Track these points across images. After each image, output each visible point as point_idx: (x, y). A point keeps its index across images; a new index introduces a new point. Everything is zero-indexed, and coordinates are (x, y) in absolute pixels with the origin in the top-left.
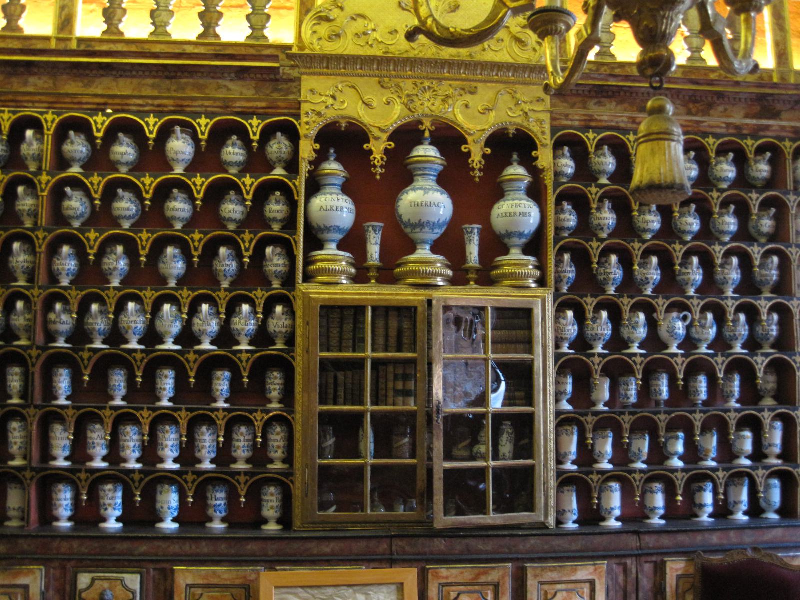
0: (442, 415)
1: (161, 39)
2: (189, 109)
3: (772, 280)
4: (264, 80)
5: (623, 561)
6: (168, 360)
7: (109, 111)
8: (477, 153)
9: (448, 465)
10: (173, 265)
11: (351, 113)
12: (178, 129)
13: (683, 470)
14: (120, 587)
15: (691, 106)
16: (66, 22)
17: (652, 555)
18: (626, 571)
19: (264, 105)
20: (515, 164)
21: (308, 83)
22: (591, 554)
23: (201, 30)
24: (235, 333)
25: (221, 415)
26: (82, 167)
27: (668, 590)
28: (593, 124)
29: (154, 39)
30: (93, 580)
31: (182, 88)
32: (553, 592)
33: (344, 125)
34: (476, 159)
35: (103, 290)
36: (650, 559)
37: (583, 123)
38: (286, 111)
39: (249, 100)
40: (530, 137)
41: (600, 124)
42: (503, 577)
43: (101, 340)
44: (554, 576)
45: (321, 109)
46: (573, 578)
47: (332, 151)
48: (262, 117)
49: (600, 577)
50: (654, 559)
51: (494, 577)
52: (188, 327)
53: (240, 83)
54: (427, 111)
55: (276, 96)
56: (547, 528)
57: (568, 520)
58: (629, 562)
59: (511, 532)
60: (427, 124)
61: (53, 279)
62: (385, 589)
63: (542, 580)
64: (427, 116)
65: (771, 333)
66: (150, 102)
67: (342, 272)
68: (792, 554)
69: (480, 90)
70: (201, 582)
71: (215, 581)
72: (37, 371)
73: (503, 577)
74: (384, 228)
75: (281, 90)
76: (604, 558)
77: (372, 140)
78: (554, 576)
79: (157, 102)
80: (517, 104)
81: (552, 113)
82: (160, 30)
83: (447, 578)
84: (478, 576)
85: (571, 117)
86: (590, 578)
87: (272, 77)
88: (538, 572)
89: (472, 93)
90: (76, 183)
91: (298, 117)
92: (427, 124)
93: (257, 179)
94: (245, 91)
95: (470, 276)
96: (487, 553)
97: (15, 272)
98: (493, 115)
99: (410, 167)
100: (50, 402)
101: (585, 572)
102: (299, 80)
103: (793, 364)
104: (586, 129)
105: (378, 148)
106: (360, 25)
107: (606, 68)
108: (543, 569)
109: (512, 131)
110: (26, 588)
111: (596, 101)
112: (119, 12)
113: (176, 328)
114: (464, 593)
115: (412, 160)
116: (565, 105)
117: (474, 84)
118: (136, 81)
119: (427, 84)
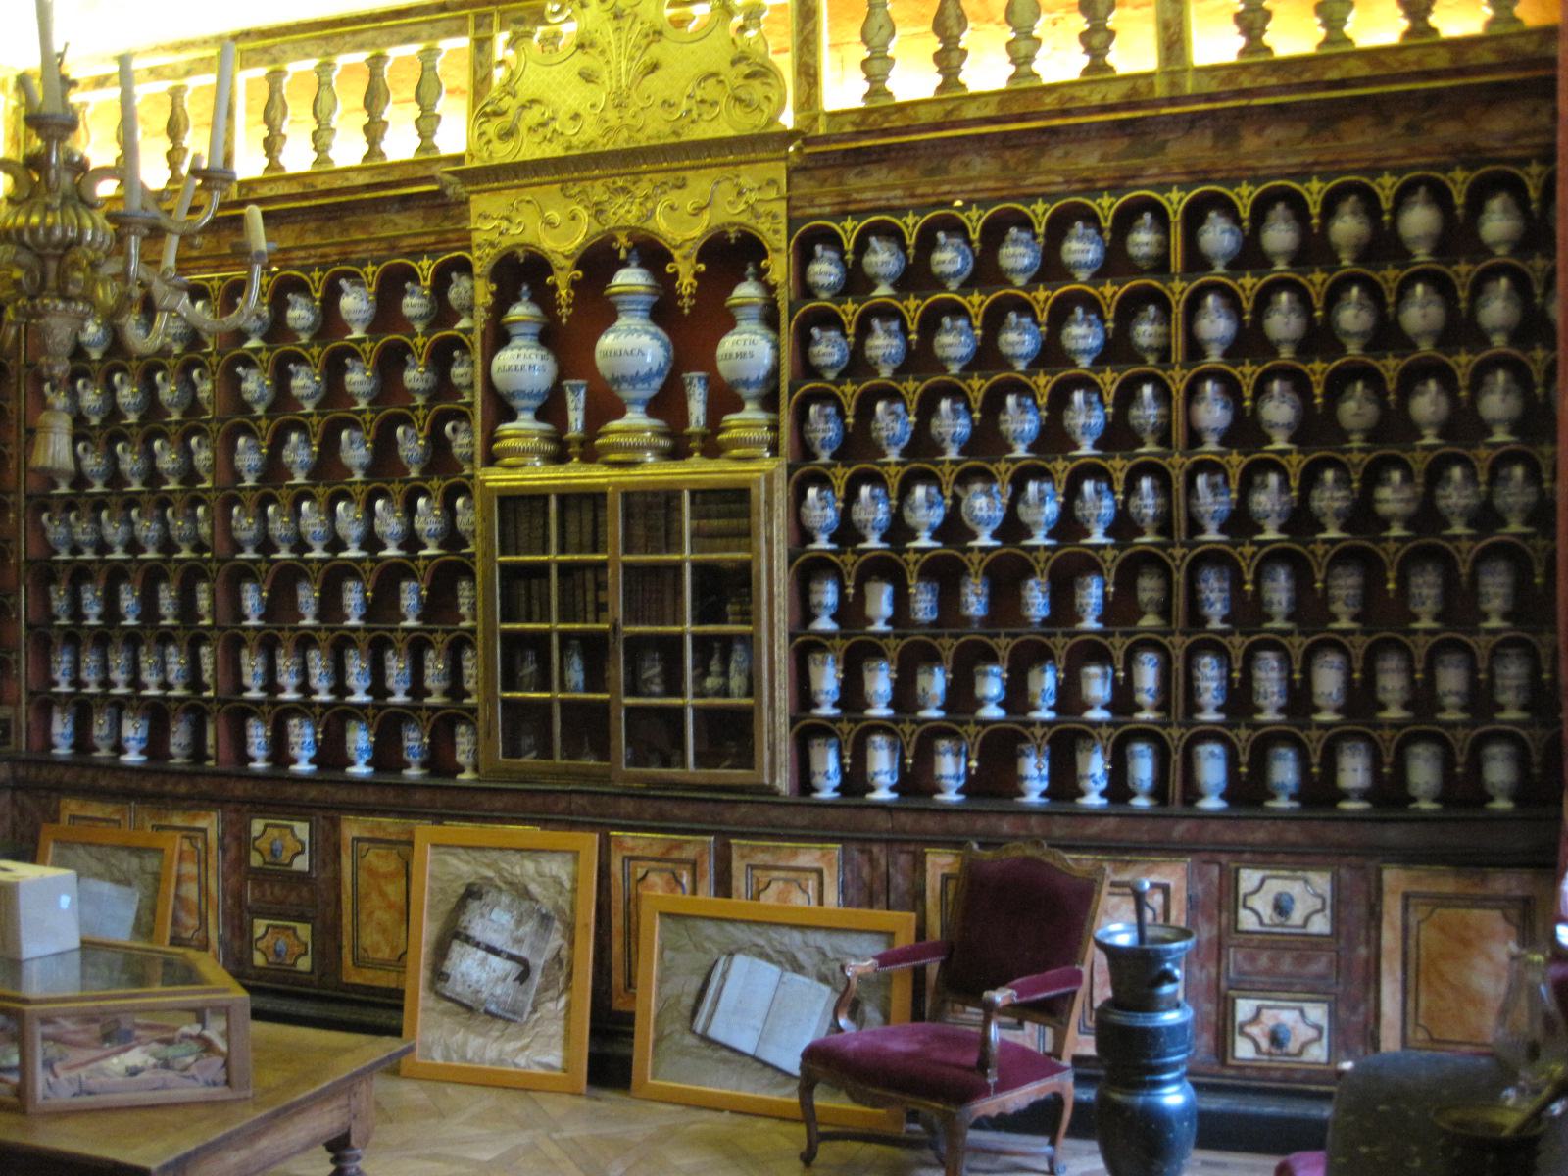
0: (621, 637)
1: (323, 168)
2: (353, 256)
3: (1147, 424)
4: (433, 207)
5: (868, 846)
6: (1214, 558)
7: (275, 269)
8: (686, 272)
9: (630, 701)
10: (351, 452)
11: (527, 238)
12: (343, 282)
13: (1109, 724)
14: (289, 837)
15: (1008, 154)
16: (1173, 41)
17: (908, 842)
18: (873, 862)
19: (432, 239)
20: (750, 279)
21: (480, 203)
22: (820, 833)
23: (939, 79)
24: (858, 525)
25: (252, 634)
26: (894, 286)
27: (929, 893)
28: (851, 207)
29: (316, 170)
30: (266, 826)
31: (345, 230)
32: (767, 880)
33: (732, 236)
34: (686, 283)
35: (1344, 451)
36: (906, 847)
37: (836, 208)
38: (459, 244)
39: (416, 235)
40: (757, 239)
41: (863, 206)
42: (701, 855)
43: (1275, 527)
44: (765, 858)
45: (494, 237)
46: (793, 864)
47: (525, 288)
48: (433, 255)
49: (830, 866)
50: (912, 847)
51: (689, 852)
52: (845, 515)
53: (407, 213)
54: (622, 223)
55: (448, 225)
56: (777, 794)
57: (1031, 790)
58: (876, 849)
59: (715, 795)
60: (623, 241)
61: (1195, 438)
62: (558, 857)
63: (752, 863)
64: (621, 229)
65: (1144, 511)
66: (312, 252)
67: (649, 447)
68: (1127, 858)
69: (689, 182)
70: (366, 835)
71: (379, 835)
72: (1179, 577)
73: (701, 855)
74: (588, 386)
75: (452, 217)
76: (832, 840)
77: (555, 270)
78: (765, 858)
79: (320, 251)
80: (740, 194)
81: (789, 199)
82: (322, 156)
83: (633, 849)
84: (669, 850)
85: (817, 202)
86: (816, 865)
87: (439, 201)
88: (746, 851)
89: (680, 188)
90: (886, 312)
91: (469, 248)
92: (623, 241)
93: (988, 296)
94: (412, 223)
95: (692, 445)
96: (685, 820)
97: (813, 444)
98: (706, 216)
99: (612, 299)
100: (1135, 623)
101: (808, 856)
102: (467, 202)
103: (1169, 560)
104: (840, 216)
105: (562, 280)
106: (533, 116)
107: (876, 115)
108: (753, 848)
109: (733, 234)
110: (204, 831)
111: (857, 170)
112: (279, 139)
113: (936, 516)
114: (654, 870)
115: (613, 290)
116: (812, 183)
117: (681, 174)
118: (297, 228)
119: (620, 183)
